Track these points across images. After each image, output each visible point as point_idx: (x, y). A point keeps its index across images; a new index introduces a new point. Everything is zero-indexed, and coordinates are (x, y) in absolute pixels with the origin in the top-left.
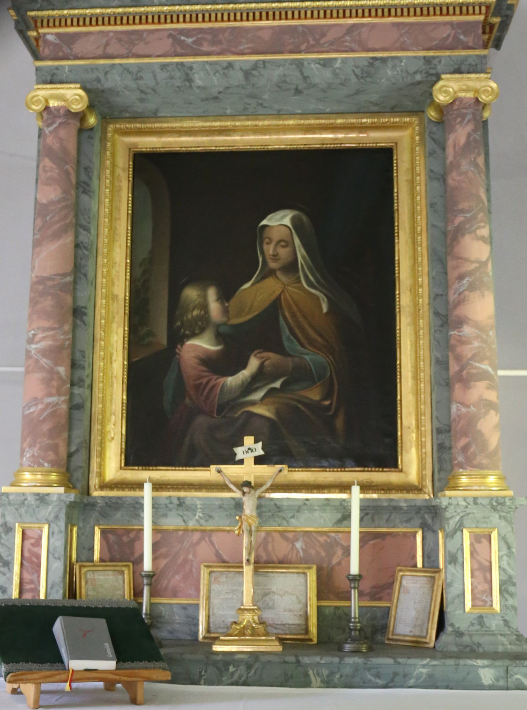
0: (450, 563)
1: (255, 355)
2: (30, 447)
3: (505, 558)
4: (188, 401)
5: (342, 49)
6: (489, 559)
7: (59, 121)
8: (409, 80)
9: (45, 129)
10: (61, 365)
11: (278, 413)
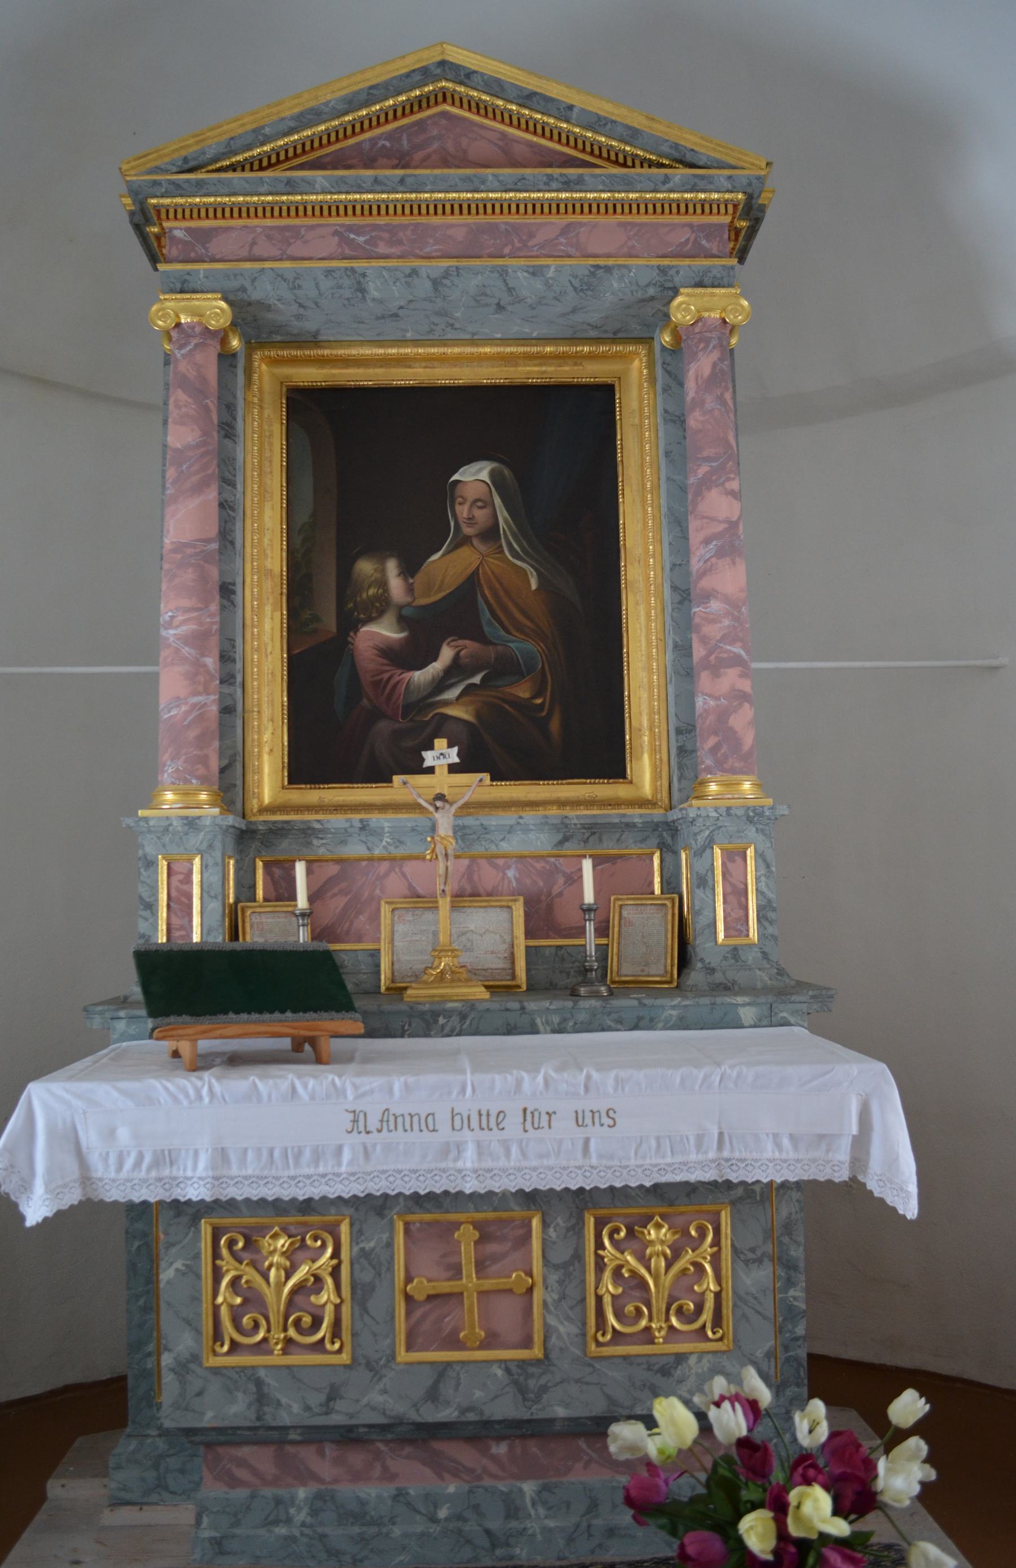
0: (698, 887)
1: (448, 644)
2: (172, 760)
3: (763, 878)
4: (365, 701)
5: (556, 254)
6: (743, 880)
7: (194, 342)
8: (640, 295)
9: (176, 352)
10: (208, 656)
11: (478, 715)
